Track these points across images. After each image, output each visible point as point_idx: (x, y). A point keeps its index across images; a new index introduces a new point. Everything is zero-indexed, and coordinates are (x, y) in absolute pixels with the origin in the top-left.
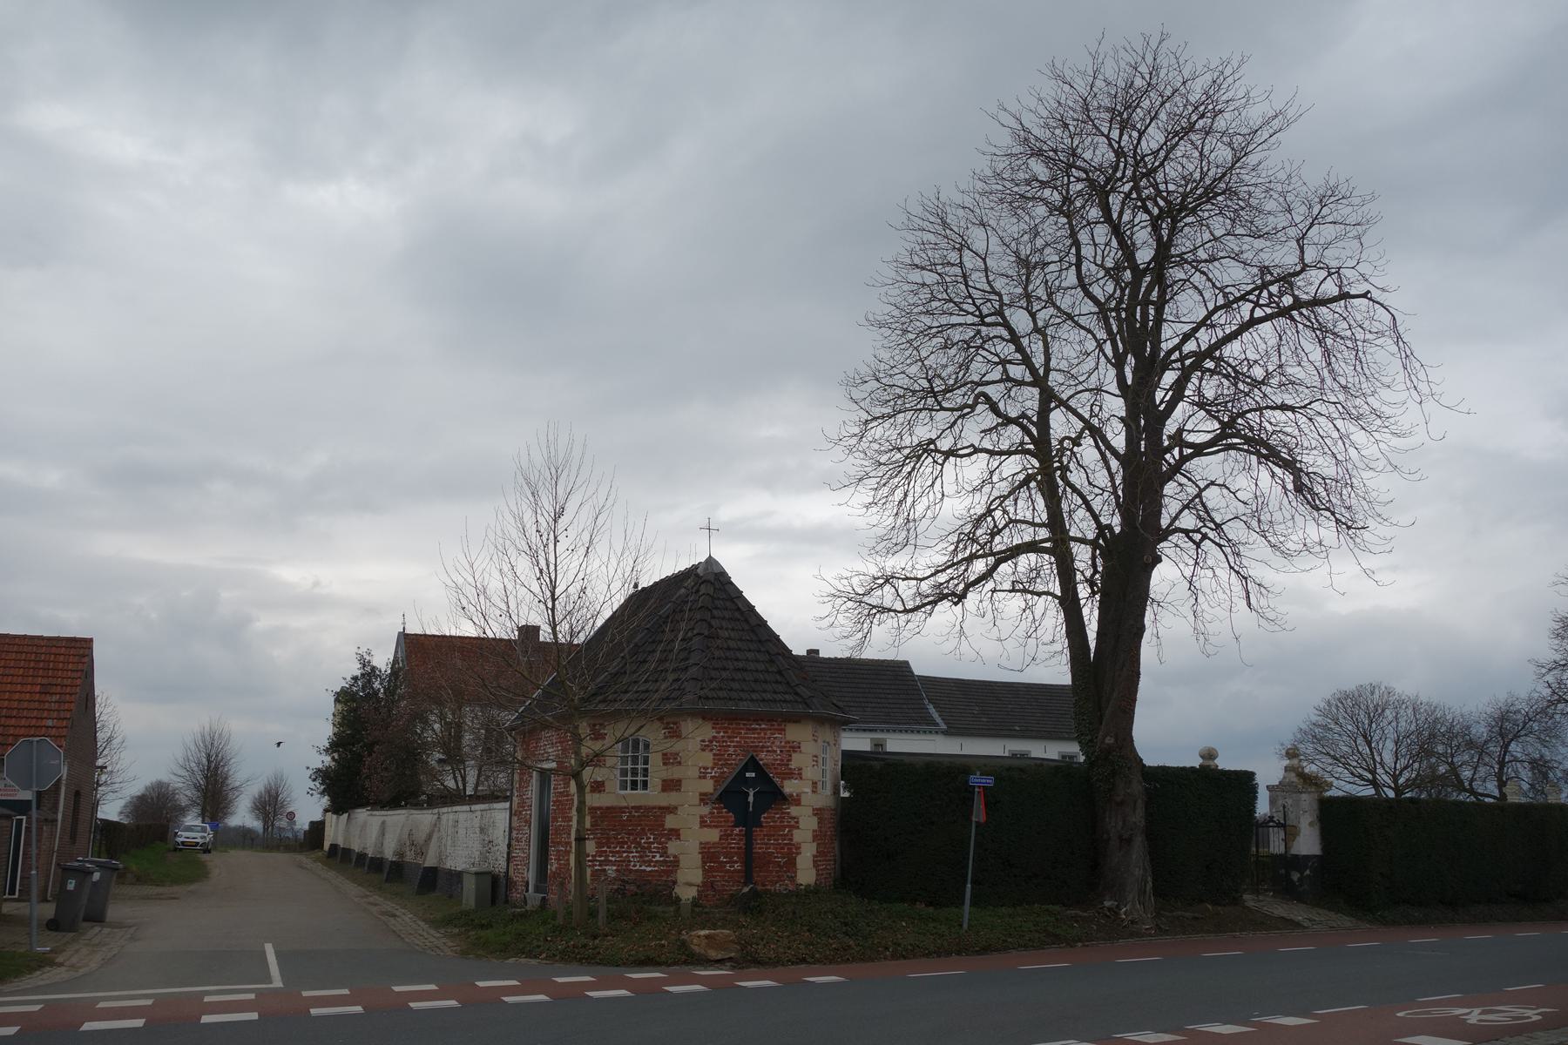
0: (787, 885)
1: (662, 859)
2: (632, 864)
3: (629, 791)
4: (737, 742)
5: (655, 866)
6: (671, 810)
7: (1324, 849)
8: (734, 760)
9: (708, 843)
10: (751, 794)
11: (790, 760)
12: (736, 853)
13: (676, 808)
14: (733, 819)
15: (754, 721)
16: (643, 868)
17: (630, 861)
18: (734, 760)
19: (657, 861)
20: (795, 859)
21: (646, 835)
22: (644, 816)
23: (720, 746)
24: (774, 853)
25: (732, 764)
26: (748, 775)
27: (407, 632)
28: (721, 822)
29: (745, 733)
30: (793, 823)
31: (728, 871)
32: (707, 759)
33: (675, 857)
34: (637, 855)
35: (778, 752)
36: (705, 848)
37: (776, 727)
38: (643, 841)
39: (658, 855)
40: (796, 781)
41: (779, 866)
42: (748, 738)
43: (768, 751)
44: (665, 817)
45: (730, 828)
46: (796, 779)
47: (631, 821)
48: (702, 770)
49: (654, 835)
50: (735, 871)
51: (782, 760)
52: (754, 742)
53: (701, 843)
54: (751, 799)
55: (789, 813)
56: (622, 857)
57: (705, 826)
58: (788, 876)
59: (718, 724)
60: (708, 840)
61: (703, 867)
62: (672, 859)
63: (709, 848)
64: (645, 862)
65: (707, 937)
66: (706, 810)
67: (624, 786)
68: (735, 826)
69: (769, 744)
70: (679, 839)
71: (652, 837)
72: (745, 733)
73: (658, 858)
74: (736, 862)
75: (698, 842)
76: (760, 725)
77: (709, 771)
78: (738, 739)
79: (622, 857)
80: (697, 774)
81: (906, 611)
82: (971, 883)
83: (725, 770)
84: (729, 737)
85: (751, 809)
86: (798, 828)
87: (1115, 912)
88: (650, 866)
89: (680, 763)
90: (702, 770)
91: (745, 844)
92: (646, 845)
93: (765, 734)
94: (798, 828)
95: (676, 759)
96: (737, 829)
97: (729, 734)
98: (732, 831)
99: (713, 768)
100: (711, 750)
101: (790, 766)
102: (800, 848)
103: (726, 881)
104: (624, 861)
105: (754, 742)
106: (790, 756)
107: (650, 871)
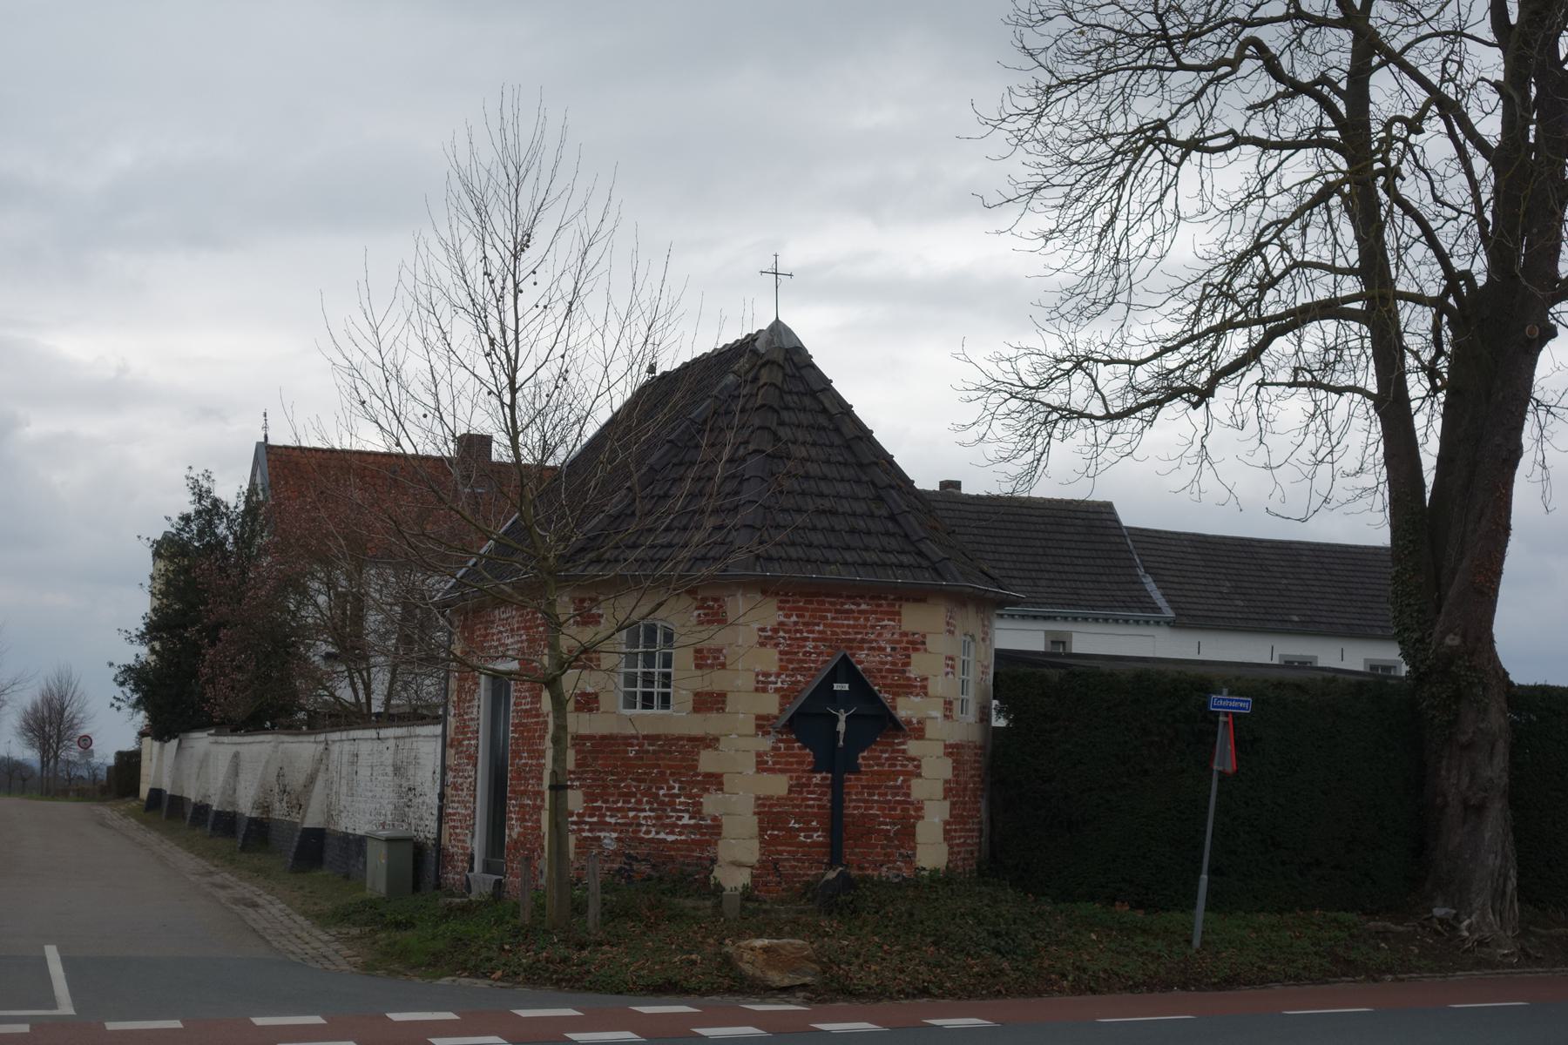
0: (899, 869)
1: (692, 822)
2: (644, 829)
3: (639, 711)
4: (819, 632)
5: (681, 834)
6: (710, 742)
8: (813, 662)
9: (771, 798)
10: (843, 717)
11: (908, 664)
12: (815, 815)
13: (717, 739)
14: (811, 759)
15: (849, 597)
16: (662, 836)
17: (640, 825)
18: (813, 662)
19: (684, 826)
20: (914, 826)
21: (667, 782)
22: (665, 752)
23: (790, 638)
24: (878, 816)
25: (810, 668)
26: (837, 687)
27: (271, 442)
28: (792, 764)
29: (833, 619)
30: (910, 767)
31: (803, 844)
32: (770, 659)
33: (715, 819)
34: (652, 814)
35: (889, 650)
36: (764, 805)
37: (885, 608)
38: (661, 792)
39: (686, 816)
40: (918, 699)
41: (887, 838)
42: (838, 626)
43: (871, 649)
44: (698, 753)
45: (806, 775)
46: (917, 695)
47: (642, 758)
48: (761, 678)
49: (681, 782)
50: (815, 844)
51: (893, 664)
52: (849, 633)
53: (758, 798)
54: (841, 727)
55: (904, 751)
56: (627, 817)
57: (765, 770)
58: (901, 854)
59: (788, 602)
60: (769, 793)
61: (761, 836)
62: (709, 822)
63: (771, 806)
64: (664, 826)
65: (766, 950)
66: (765, 744)
67: (666, 700)
68: (814, 771)
69: (873, 637)
70: (722, 790)
71: (677, 785)
72: (833, 619)
73: (686, 821)
74: (816, 830)
75: (753, 795)
76: (859, 605)
77: (772, 679)
78: (821, 628)
79: (627, 817)
80: (753, 685)
81: (1109, 417)
82: (1208, 874)
83: (799, 678)
84: (805, 624)
85: (841, 743)
86: (919, 775)
87: (1451, 925)
88: (672, 833)
89: (723, 666)
90: (761, 678)
91: (832, 801)
92: (667, 799)
93: (867, 619)
94: (919, 775)
95: (718, 658)
96: (819, 776)
97: (806, 620)
98: (809, 779)
99: (778, 675)
100: (777, 645)
101: (907, 675)
102: (921, 808)
103: (798, 860)
104: (630, 825)
105: (849, 633)
106: (908, 657)
107: (672, 842)
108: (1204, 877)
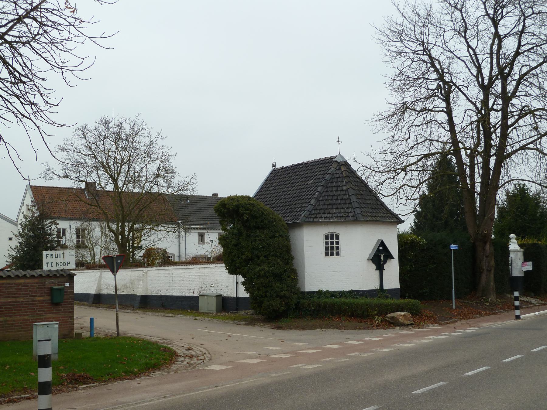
7: (400, 286)
54: (382, 258)
108: (453, 290)
